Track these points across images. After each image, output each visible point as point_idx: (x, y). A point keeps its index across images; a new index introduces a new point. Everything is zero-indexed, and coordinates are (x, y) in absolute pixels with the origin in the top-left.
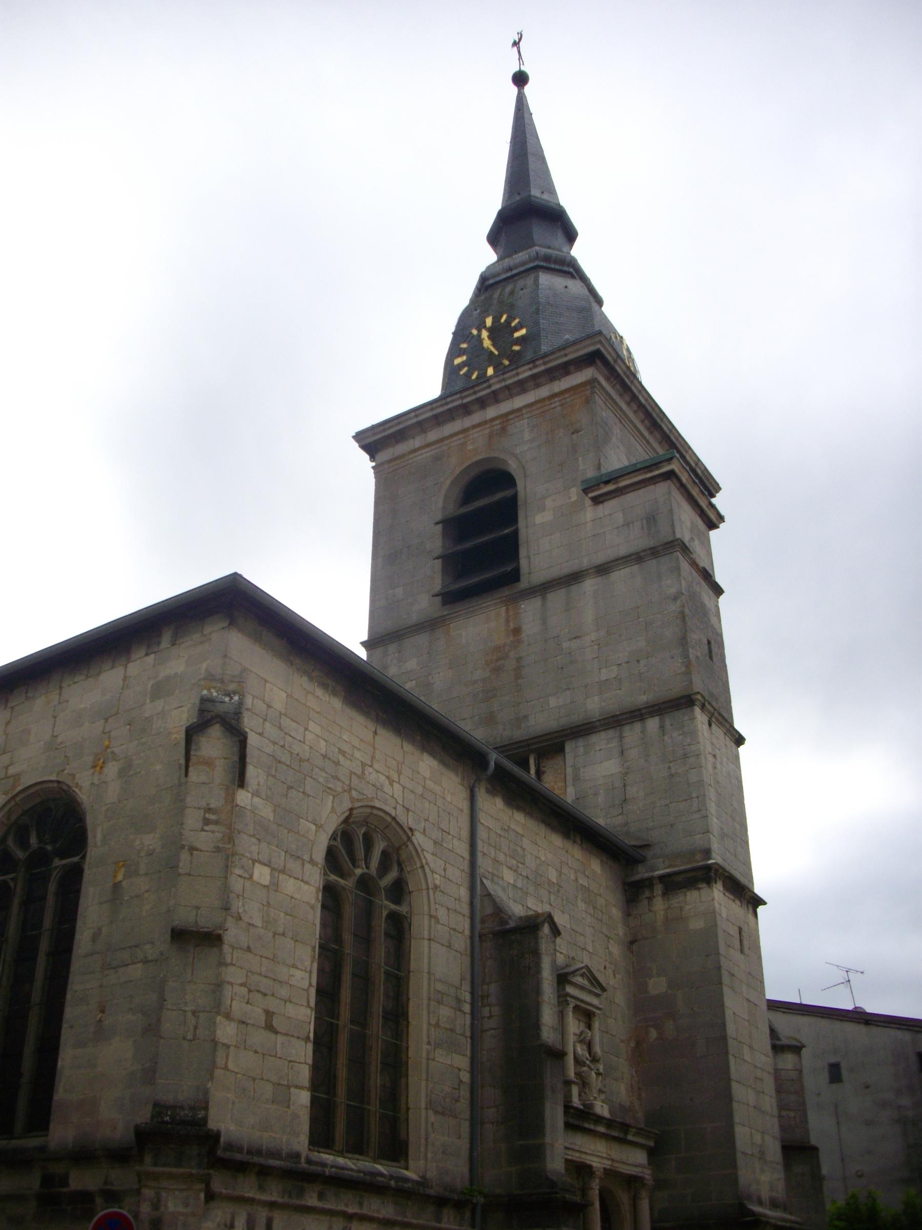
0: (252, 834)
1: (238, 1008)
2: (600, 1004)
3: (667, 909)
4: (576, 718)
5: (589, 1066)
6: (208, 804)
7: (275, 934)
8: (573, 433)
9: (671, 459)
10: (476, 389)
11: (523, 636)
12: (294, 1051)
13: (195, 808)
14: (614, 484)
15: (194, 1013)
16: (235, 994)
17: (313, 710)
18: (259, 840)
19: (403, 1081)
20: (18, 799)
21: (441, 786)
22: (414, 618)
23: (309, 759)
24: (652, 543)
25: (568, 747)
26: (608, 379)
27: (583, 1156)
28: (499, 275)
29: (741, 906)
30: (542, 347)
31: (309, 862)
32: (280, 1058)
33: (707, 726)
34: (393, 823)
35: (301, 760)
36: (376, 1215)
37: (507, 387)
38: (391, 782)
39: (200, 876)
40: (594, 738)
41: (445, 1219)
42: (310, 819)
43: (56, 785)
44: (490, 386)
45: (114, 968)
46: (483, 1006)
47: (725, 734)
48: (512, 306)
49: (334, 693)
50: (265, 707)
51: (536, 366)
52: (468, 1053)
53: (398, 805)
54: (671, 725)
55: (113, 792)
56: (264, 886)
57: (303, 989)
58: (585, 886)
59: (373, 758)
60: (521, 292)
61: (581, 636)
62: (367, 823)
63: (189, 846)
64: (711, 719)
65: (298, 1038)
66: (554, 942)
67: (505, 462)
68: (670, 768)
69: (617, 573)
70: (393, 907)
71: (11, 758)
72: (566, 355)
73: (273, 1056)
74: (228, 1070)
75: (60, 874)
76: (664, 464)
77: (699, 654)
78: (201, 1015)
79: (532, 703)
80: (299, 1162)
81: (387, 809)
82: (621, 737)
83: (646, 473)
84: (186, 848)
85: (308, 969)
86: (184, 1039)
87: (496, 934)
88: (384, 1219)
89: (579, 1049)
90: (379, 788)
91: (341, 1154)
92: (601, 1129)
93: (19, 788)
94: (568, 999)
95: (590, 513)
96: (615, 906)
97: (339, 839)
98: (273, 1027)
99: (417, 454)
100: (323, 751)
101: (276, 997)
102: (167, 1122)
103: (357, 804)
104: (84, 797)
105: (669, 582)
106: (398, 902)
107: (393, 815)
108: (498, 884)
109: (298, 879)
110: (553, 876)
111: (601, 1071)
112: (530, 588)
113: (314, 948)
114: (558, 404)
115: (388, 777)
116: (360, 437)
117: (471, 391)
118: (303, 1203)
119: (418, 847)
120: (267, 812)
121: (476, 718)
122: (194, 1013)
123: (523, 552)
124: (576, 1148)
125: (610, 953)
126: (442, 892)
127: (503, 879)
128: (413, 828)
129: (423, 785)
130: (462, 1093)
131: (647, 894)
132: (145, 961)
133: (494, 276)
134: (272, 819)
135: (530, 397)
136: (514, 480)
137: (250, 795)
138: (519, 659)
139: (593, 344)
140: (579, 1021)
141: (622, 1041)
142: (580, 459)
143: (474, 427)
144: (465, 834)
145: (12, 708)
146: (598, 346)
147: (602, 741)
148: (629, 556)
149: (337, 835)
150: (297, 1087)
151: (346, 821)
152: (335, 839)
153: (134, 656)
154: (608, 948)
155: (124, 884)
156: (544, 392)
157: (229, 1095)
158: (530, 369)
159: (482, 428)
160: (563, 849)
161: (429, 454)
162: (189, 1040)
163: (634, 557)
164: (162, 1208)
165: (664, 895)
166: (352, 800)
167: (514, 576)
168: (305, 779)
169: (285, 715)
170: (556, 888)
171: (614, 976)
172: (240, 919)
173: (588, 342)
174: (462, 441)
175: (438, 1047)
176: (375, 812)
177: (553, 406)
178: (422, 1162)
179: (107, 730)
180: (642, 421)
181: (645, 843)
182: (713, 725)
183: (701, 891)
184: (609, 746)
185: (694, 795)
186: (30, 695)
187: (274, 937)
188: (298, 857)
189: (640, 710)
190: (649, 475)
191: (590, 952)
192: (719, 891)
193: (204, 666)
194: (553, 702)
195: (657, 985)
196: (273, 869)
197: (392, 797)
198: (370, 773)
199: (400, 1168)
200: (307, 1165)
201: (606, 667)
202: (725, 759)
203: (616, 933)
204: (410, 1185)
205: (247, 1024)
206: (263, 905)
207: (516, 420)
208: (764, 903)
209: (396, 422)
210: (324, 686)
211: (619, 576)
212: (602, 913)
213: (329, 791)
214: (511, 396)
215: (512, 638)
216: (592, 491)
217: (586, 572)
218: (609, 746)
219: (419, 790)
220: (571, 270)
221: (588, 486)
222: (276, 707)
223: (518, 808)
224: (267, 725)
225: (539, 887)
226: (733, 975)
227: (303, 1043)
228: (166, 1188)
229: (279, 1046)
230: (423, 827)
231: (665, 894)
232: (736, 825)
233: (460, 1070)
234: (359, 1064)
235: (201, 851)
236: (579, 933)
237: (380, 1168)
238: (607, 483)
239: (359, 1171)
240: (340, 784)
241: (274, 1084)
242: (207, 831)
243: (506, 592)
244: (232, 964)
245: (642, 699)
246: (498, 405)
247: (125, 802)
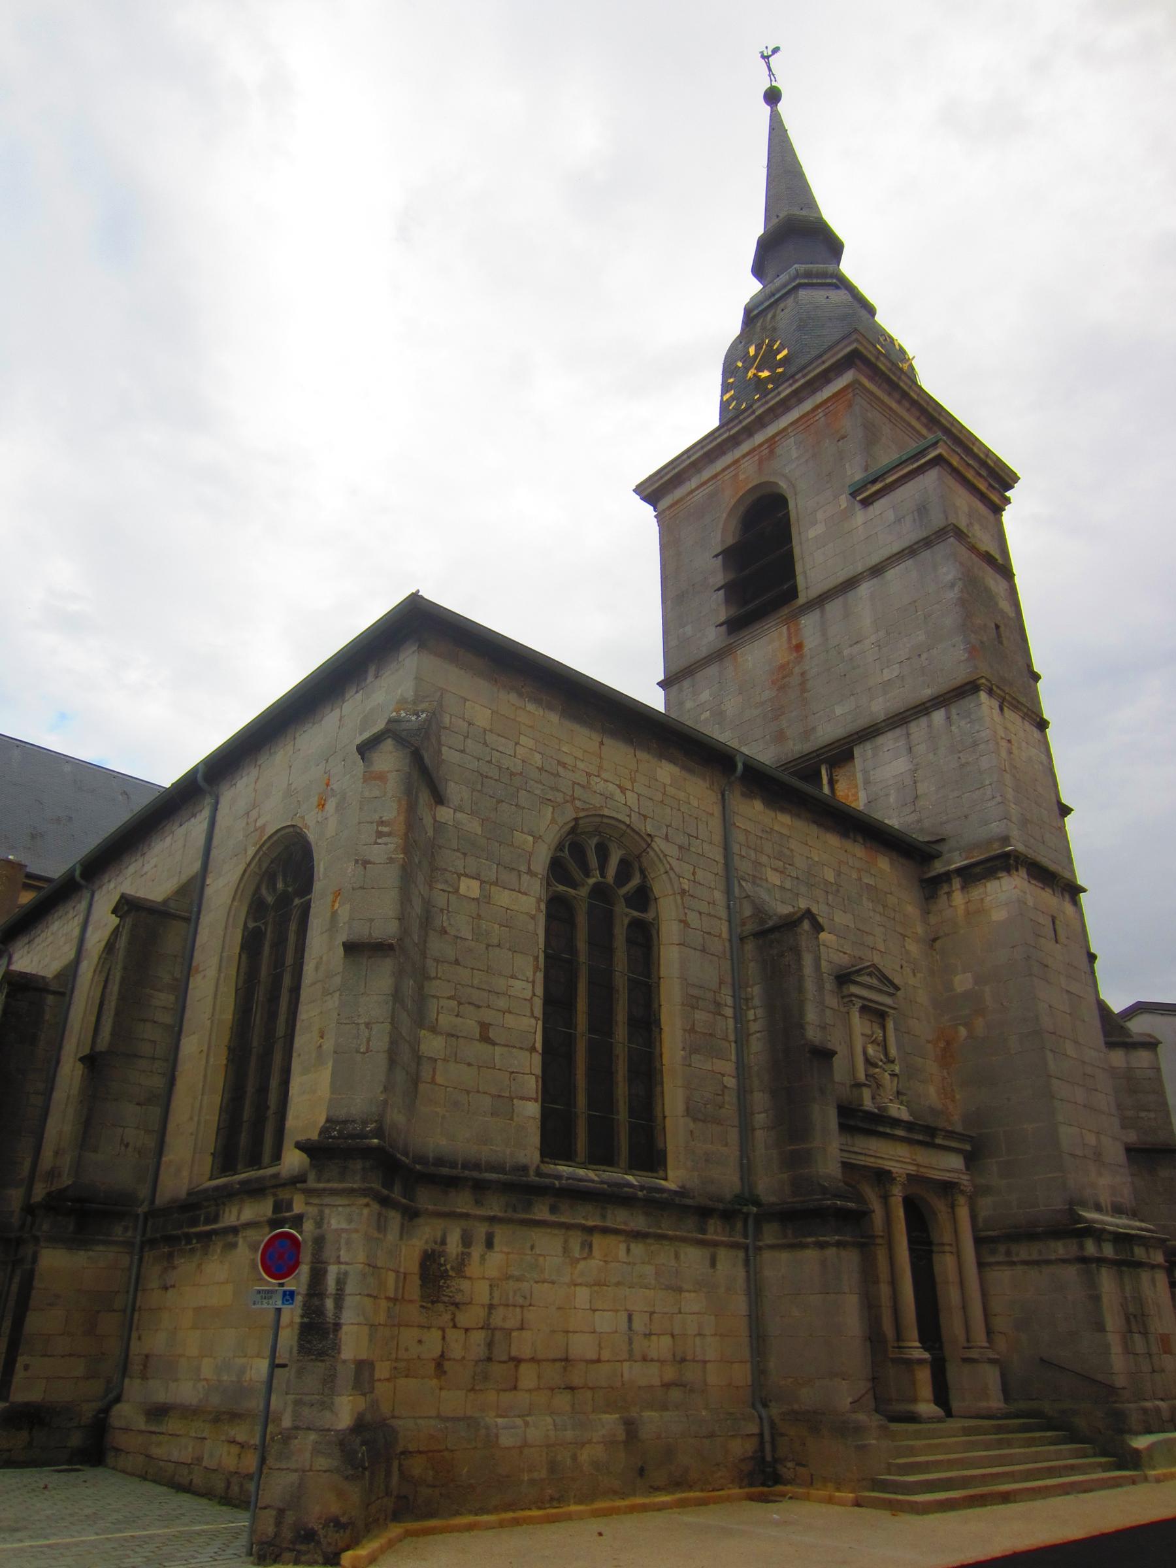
0: (456, 848)
1: (445, 1021)
2: (894, 1003)
3: (967, 903)
4: (863, 722)
5: (881, 1067)
6: (381, 818)
7: (488, 946)
8: (839, 441)
9: (936, 443)
10: (741, 418)
11: (806, 650)
12: (516, 1062)
13: (368, 823)
14: (881, 481)
15: (368, 1025)
16: (442, 1007)
17: (524, 724)
18: (465, 854)
19: (658, 1089)
20: (264, 849)
21: (685, 792)
22: (704, 652)
23: (521, 773)
24: (925, 535)
25: (857, 752)
26: (871, 379)
27: (880, 1161)
28: (762, 303)
29: (1054, 894)
31: (527, 873)
32: (499, 1069)
33: (998, 711)
34: (628, 831)
35: (512, 774)
36: (622, 1227)
37: (771, 409)
38: (623, 790)
39: (373, 888)
40: (880, 740)
41: (711, 1229)
42: (525, 830)
43: (291, 829)
44: (753, 412)
45: (331, 994)
46: (748, 1009)
47: (1023, 718)
48: (774, 329)
49: (550, 707)
50: (466, 724)
51: (796, 381)
52: (733, 1058)
53: (632, 813)
54: (958, 714)
55: (332, 827)
56: (473, 899)
57: (526, 1000)
58: (871, 885)
59: (600, 768)
60: (782, 313)
61: (861, 641)
62: (600, 832)
63: (362, 860)
64: (1002, 703)
65: (521, 1048)
66: (817, 938)
67: (776, 484)
68: (959, 758)
69: (892, 571)
70: (635, 914)
71: (505, 868)
72: (824, 362)
73: (491, 1068)
74: (436, 1084)
75: (299, 912)
76: (930, 450)
77: (985, 639)
78: (374, 1026)
79: (818, 714)
80: (527, 1175)
81: (620, 817)
82: (908, 734)
83: (912, 464)
84: (360, 862)
85: (531, 980)
86: (358, 1051)
87: (759, 935)
88: (632, 1231)
89: (871, 1050)
90: (608, 797)
91: (582, 1165)
92: (900, 1132)
93: (265, 837)
94: (853, 999)
95: (861, 516)
96: (910, 903)
97: (566, 850)
98: (490, 1038)
99: (694, 494)
100: (539, 764)
101: (493, 1009)
102: (334, 1137)
103: (582, 814)
104: (311, 837)
105: (945, 570)
106: (644, 909)
107: (628, 823)
108: (761, 886)
109: (514, 890)
110: (830, 876)
111: (897, 1072)
112: (808, 603)
113: (536, 958)
114: (821, 415)
115: (619, 786)
116: (639, 490)
117: (737, 421)
118: (530, 1217)
119: (659, 853)
120: (474, 826)
122: (368, 1025)
123: (799, 569)
124: (871, 1153)
125: (908, 952)
126: (692, 896)
127: (767, 881)
128: (653, 834)
129: (663, 791)
130: (727, 1098)
131: (946, 888)
133: (757, 306)
134: (480, 833)
135: (794, 415)
136: (787, 500)
137: (452, 811)
139: (849, 344)
140: (872, 1021)
141: (928, 1042)
143: (744, 456)
144: (717, 838)
145: (260, 766)
146: (854, 345)
147: (889, 741)
148: (903, 550)
149: (564, 846)
150: (523, 1098)
151: (573, 830)
152: (562, 850)
153: (347, 696)
154: (904, 947)
155: (339, 911)
156: (807, 406)
157: (438, 1110)
158: (791, 385)
159: (752, 455)
160: (840, 848)
162: (361, 1053)
163: (906, 552)
164: (325, 1226)
165: (963, 888)
166: (577, 809)
167: (793, 593)
168: (518, 792)
169: (491, 731)
170: (834, 888)
171: (914, 975)
172: (446, 932)
173: (845, 342)
175: (695, 1053)
176: (605, 820)
177: (817, 418)
179: (328, 769)
180: (918, 419)
181: (939, 838)
182: (1005, 708)
183: (1002, 880)
184: (897, 745)
185: (987, 783)
186: (272, 751)
187: (487, 949)
188: (513, 869)
189: (924, 703)
190: (915, 465)
191: (881, 952)
192: (1023, 878)
194: (839, 711)
195: (962, 982)
196: (482, 882)
197: (626, 805)
198: (597, 783)
199: (657, 1178)
200: (537, 1178)
201: (888, 667)
202: (1024, 744)
203: (914, 931)
204: (665, 1195)
205: (458, 1037)
206: (473, 918)
208: (1084, 890)
209: (671, 467)
210: (537, 701)
212: (895, 911)
213: (548, 802)
214: (777, 417)
215: (795, 655)
216: (860, 494)
217: (860, 577)
218: (897, 745)
219: (658, 797)
221: (854, 489)
222: (478, 724)
223: (783, 810)
224: (469, 741)
225: (813, 888)
226: (1046, 966)
227: (528, 1054)
228: (329, 1205)
229: (497, 1058)
230: (665, 833)
231: (964, 888)
232: (1043, 810)
233: (723, 1075)
234: (601, 1072)
235: (374, 864)
236: (866, 933)
237: (630, 1178)
238: (874, 482)
239: (602, 1182)
240: (561, 795)
241: (493, 1096)
242: (380, 844)
243: (785, 611)
244: (436, 978)
245: (927, 692)
246: (764, 430)
247: (341, 834)
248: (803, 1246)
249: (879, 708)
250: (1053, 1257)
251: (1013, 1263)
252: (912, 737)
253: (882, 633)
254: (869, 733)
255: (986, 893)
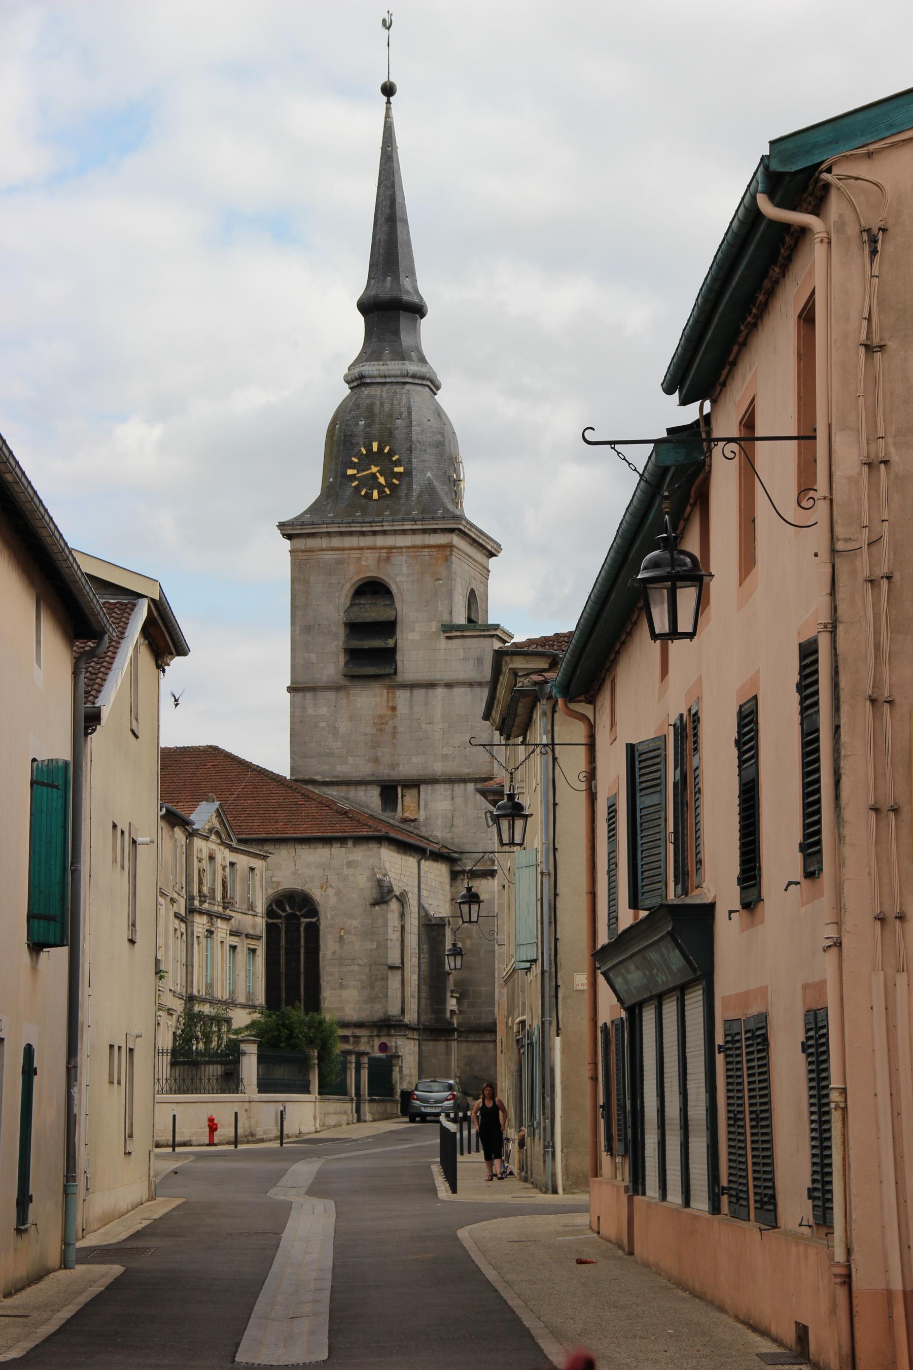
11: (398, 713)
30: (414, 486)
40: (437, 787)
82: (453, 790)
95: (443, 643)
114: (427, 553)
116: (282, 526)
117: (369, 525)
121: (367, 757)
131: (462, 877)
132: (359, 965)
138: (394, 727)
142: (439, 602)
155: (345, 936)
158: (412, 525)
161: (333, 556)
174: (358, 556)
178: (409, 1016)
193: (371, 860)
207: (398, 554)
211: (458, 691)
215: (390, 712)
220: (429, 383)
243: (387, 682)
245: (465, 771)
248: (440, 1040)
249: (439, 768)
250: (485, 1040)
251: (468, 1041)
252: (454, 792)
253: (446, 725)
254: (433, 781)
255: (480, 884)
